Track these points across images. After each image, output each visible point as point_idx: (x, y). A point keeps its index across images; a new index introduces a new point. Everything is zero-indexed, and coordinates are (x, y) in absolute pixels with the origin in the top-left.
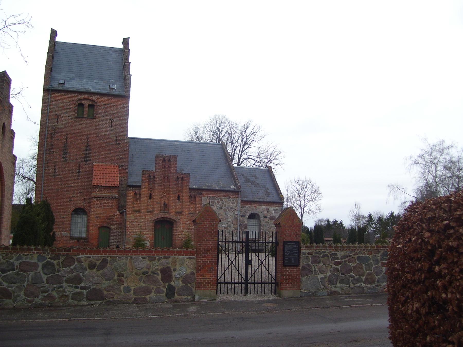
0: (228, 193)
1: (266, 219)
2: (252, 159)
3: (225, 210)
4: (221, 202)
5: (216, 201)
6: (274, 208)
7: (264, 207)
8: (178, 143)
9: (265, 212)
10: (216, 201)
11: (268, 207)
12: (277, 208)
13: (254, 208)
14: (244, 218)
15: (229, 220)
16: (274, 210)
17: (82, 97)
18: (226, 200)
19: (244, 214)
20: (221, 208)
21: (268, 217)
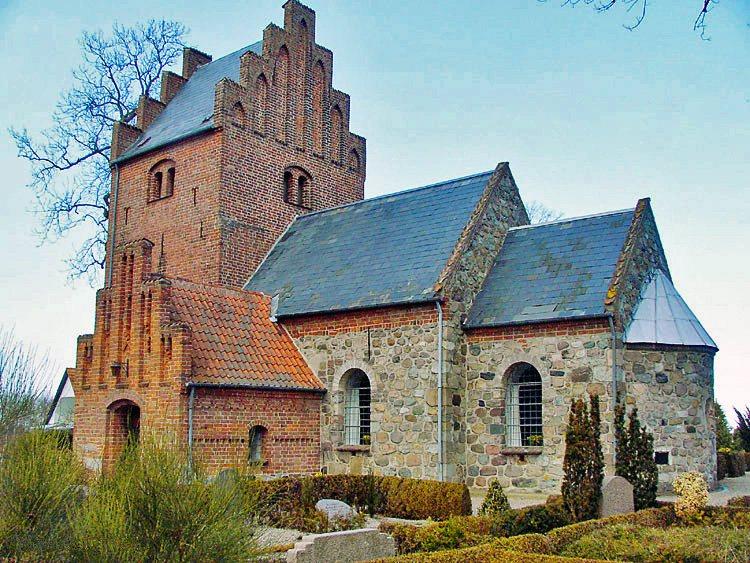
0: (413, 311)
1: (557, 380)
2: (101, 80)
3: (407, 365)
4: (396, 340)
5: (384, 340)
6: (586, 338)
7: (552, 340)
8: (393, 200)
9: (557, 357)
10: (384, 340)
11: (561, 339)
12: (595, 337)
13: (520, 346)
14: (490, 382)
15: (419, 393)
16: (587, 345)
17: (155, 160)
18: (408, 333)
19: (491, 368)
20: (397, 360)
21: (567, 371)
